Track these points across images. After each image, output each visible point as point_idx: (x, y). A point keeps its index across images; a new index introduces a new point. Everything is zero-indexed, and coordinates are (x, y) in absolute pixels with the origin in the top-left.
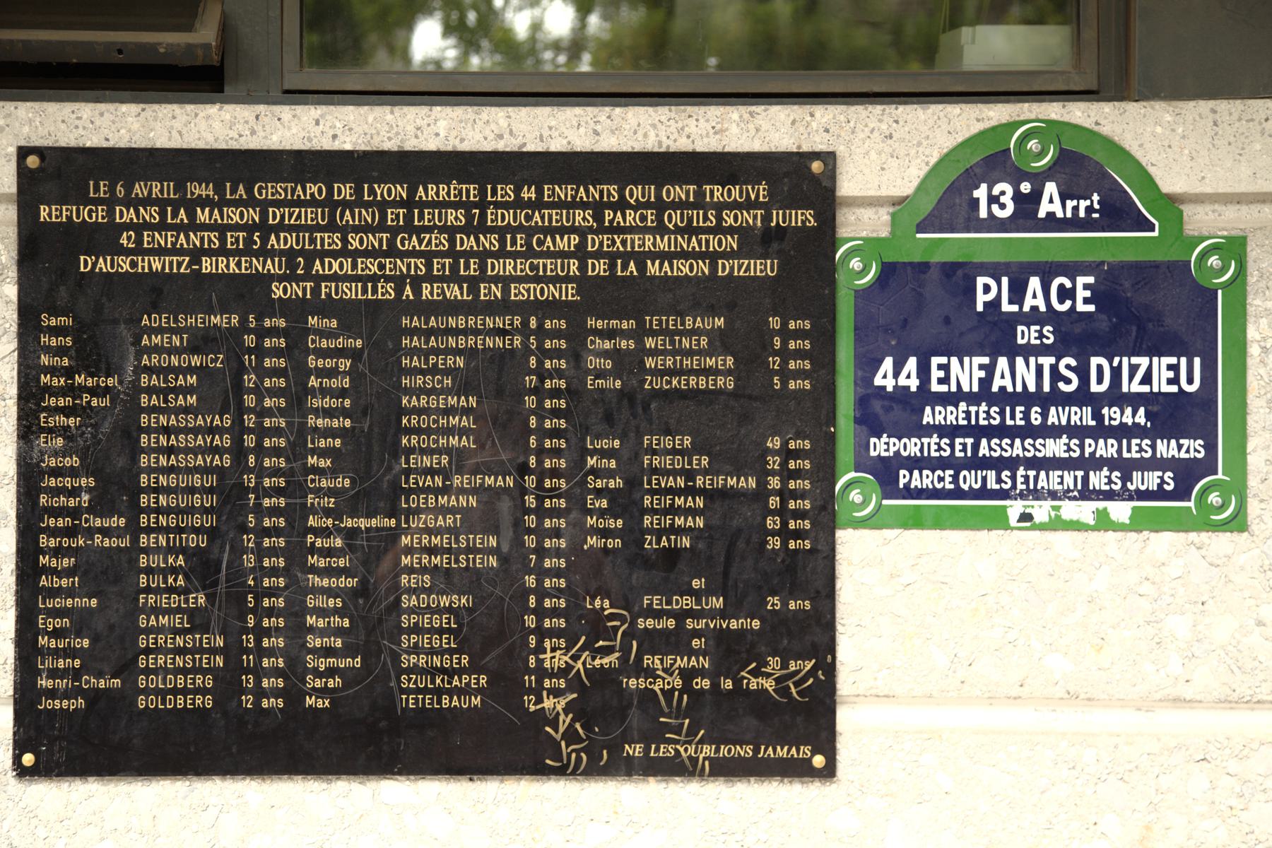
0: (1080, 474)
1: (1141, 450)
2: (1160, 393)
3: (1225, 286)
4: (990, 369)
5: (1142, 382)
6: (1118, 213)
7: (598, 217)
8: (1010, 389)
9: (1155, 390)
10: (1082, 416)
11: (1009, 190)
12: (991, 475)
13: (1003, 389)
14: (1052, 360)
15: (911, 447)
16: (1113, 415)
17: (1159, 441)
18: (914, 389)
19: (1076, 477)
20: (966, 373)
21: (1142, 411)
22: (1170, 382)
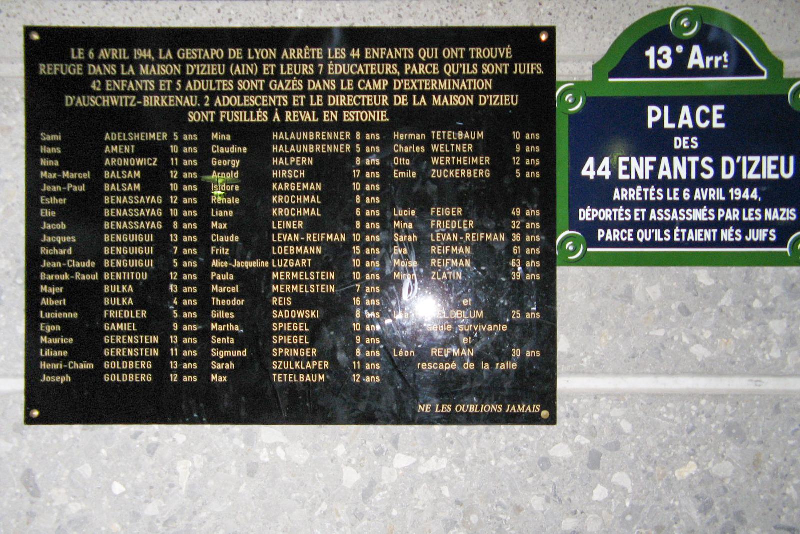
1: (755, 215)
4: (657, 165)
7: (401, 68)
8: (670, 177)
9: (764, 177)
10: (717, 194)
12: (658, 232)
13: (665, 177)
14: (697, 158)
15: (606, 214)
16: (736, 193)
18: (607, 177)
20: (642, 167)
21: (755, 190)
22: (774, 172)
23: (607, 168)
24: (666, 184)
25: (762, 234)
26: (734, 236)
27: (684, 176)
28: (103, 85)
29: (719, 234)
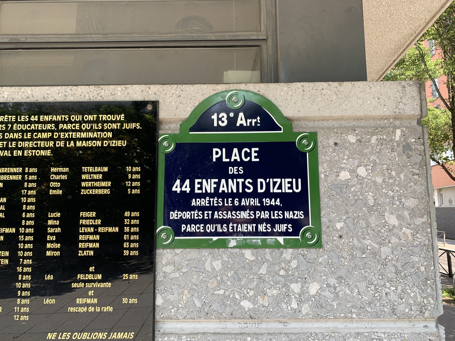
0: (254, 225)
1: (278, 215)
4: (218, 184)
5: (278, 188)
8: (226, 191)
9: (284, 191)
10: (255, 202)
11: (225, 116)
13: (223, 191)
14: (243, 180)
15: (187, 215)
16: (267, 201)
17: (285, 212)
18: (188, 192)
19: (253, 227)
20: (209, 185)
21: (278, 200)
22: (289, 188)
24: (224, 196)
25: (283, 227)
26: (267, 228)
27: (235, 191)
29: (257, 227)
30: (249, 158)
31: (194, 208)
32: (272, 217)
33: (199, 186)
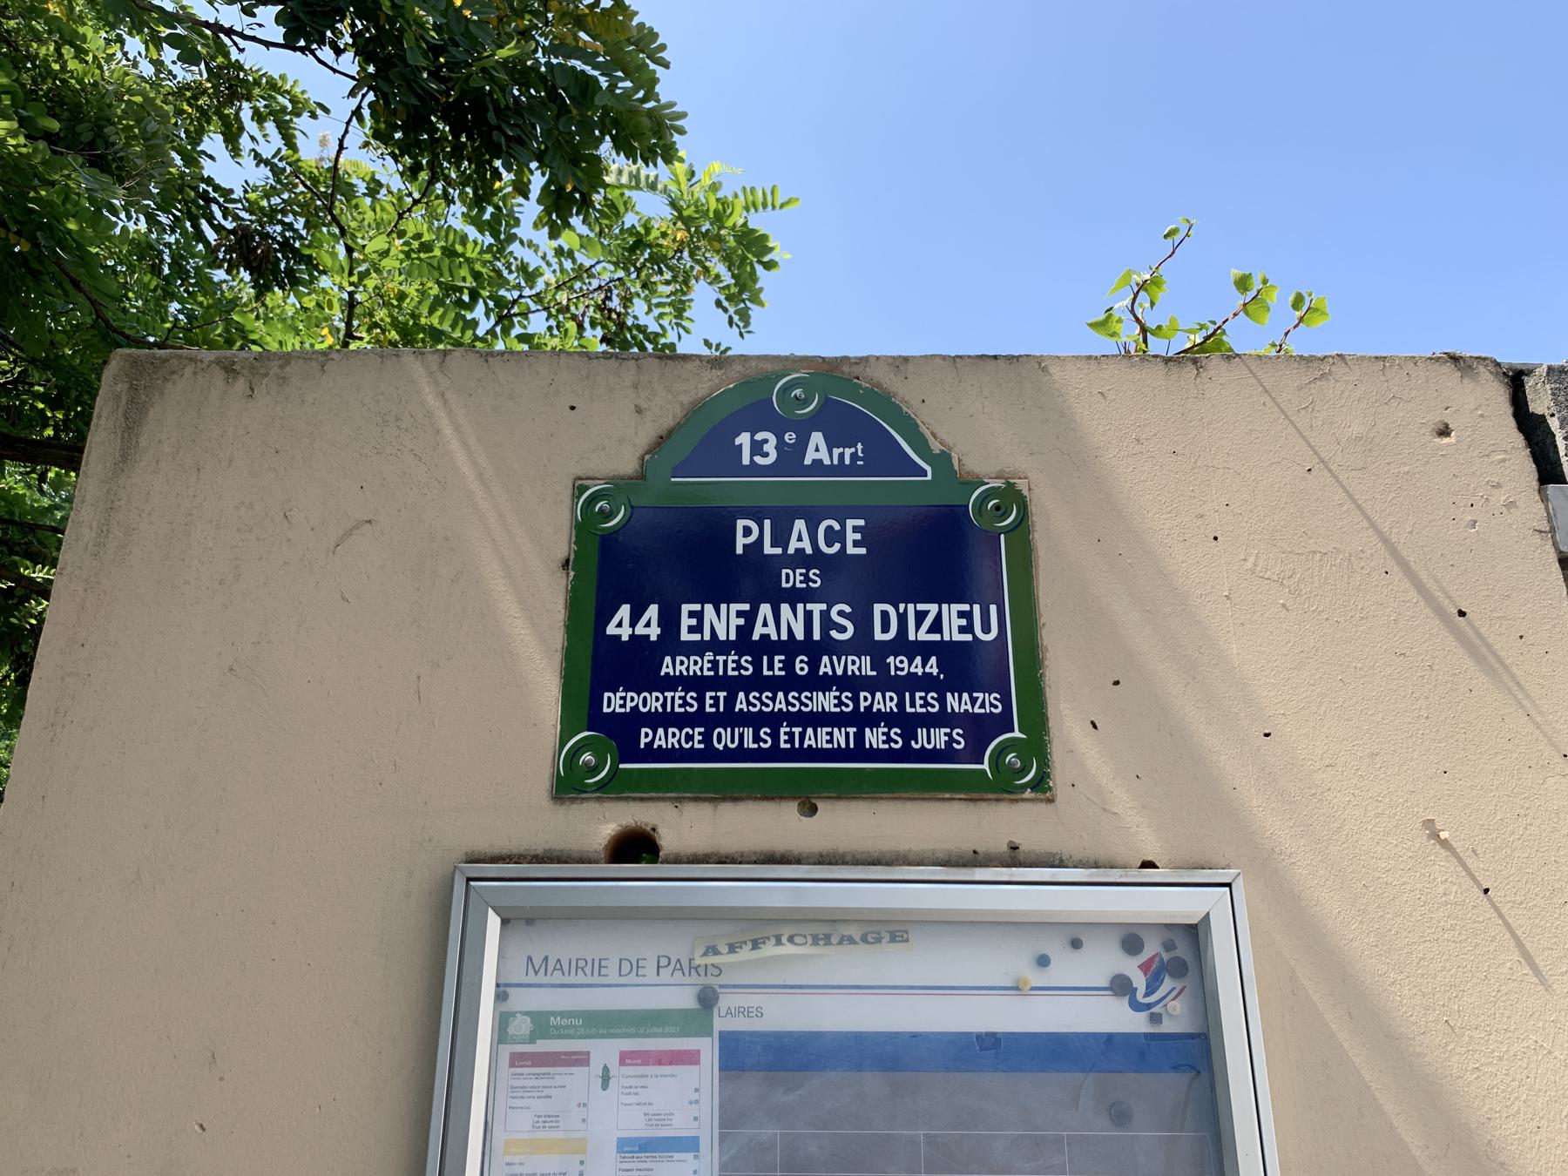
0: (852, 730)
1: (926, 704)
2: (951, 641)
3: (1008, 531)
4: (750, 617)
6: (884, 457)
8: (774, 637)
9: (947, 638)
10: (862, 666)
11: (773, 440)
12: (749, 733)
13: (765, 637)
14: (824, 607)
15: (653, 702)
17: (949, 695)
18: (653, 638)
19: (847, 734)
20: (723, 621)
21: (933, 660)
22: (962, 630)
23: (654, 623)
25: (939, 738)
26: (889, 740)
27: (800, 636)
28: (788, 665)
29: (860, 737)
30: (837, 546)
31: (671, 683)
32: (909, 710)
33: (694, 622)
